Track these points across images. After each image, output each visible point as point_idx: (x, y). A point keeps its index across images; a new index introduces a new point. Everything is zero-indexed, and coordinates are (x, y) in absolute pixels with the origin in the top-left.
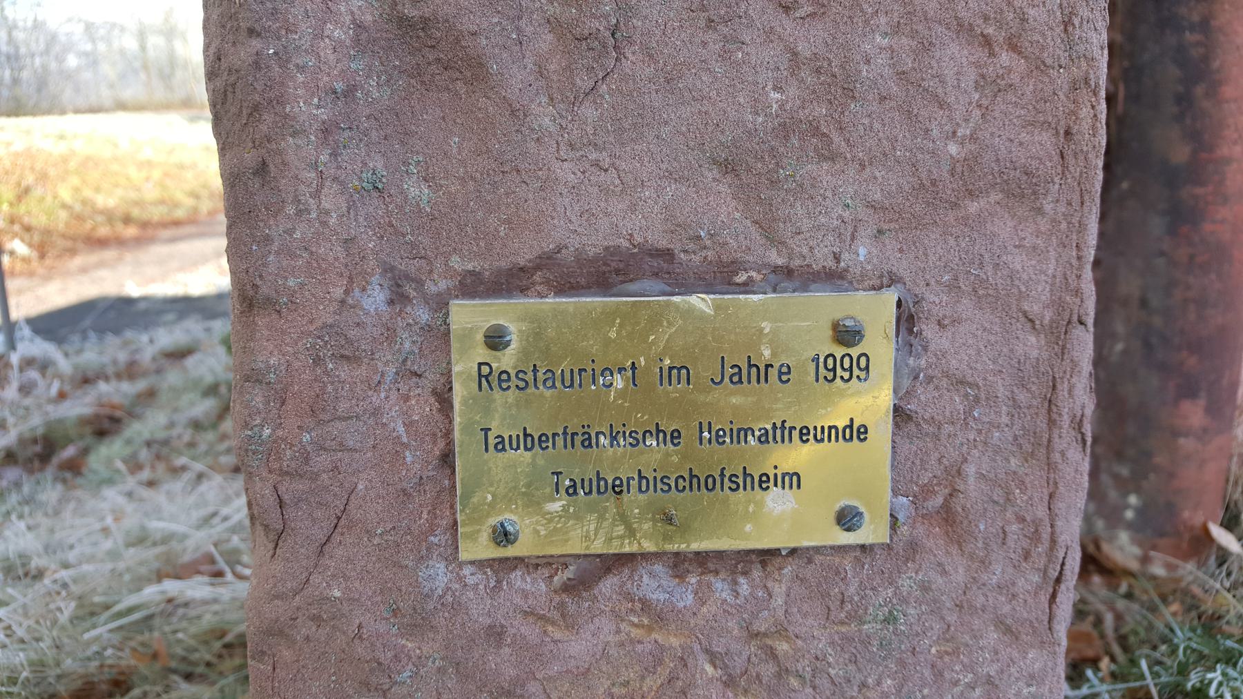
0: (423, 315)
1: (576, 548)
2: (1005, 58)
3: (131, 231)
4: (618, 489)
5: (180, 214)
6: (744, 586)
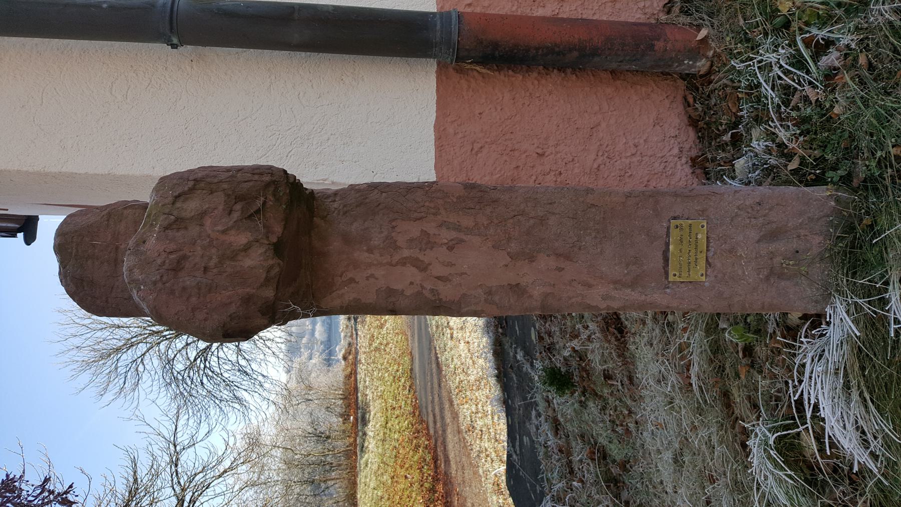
0: (671, 284)
1: (705, 265)
2: (640, 205)
3: (440, 487)
4: (696, 259)
5: (428, 458)
6: (711, 241)
